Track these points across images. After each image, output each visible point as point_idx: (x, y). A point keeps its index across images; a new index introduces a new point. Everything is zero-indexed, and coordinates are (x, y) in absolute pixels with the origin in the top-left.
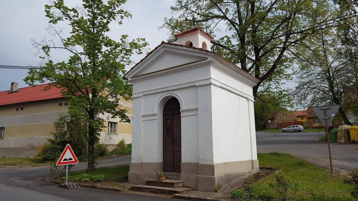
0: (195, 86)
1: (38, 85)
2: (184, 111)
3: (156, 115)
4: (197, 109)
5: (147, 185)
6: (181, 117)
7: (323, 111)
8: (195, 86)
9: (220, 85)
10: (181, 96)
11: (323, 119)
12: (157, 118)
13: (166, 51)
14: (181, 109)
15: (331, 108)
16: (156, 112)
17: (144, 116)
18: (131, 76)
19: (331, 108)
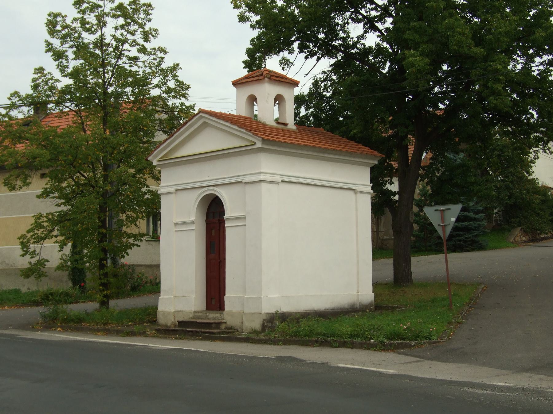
0: (241, 182)
1: (19, 118)
2: (228, 219)
3: (192, 223)
4: (244, 218)
5: (14, 335)
6: (226, 229)
7: (439, 214)
8: (241, 182)
9: (278, 179)
10: (224, 194)
11: (439, 225)
12: (194, 228)
13: (205, 123)
14: (226, 216)
15: (450, 209)
16: (193, 218)
17: (176, 224)
18: (158, 158)
19: (450, 209)
